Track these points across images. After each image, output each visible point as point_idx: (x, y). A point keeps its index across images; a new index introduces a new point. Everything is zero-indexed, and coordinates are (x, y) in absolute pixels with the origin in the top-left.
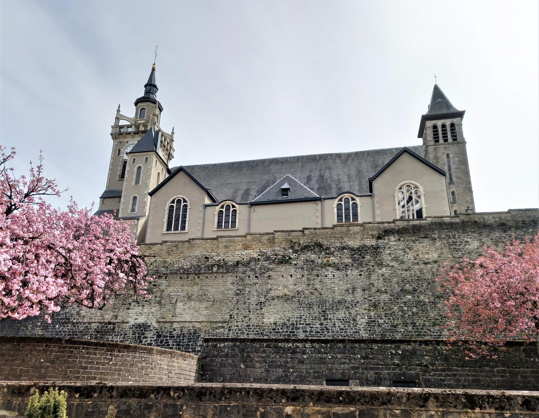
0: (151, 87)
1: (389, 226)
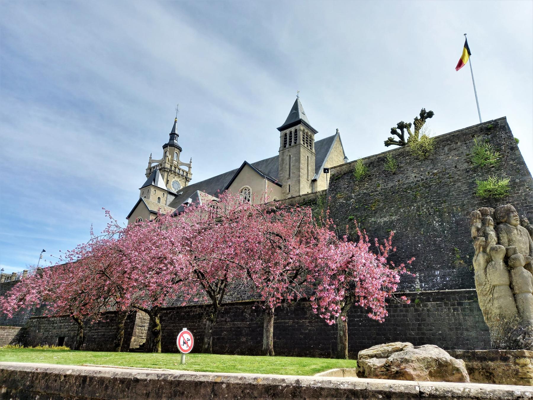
1: (342, 170)
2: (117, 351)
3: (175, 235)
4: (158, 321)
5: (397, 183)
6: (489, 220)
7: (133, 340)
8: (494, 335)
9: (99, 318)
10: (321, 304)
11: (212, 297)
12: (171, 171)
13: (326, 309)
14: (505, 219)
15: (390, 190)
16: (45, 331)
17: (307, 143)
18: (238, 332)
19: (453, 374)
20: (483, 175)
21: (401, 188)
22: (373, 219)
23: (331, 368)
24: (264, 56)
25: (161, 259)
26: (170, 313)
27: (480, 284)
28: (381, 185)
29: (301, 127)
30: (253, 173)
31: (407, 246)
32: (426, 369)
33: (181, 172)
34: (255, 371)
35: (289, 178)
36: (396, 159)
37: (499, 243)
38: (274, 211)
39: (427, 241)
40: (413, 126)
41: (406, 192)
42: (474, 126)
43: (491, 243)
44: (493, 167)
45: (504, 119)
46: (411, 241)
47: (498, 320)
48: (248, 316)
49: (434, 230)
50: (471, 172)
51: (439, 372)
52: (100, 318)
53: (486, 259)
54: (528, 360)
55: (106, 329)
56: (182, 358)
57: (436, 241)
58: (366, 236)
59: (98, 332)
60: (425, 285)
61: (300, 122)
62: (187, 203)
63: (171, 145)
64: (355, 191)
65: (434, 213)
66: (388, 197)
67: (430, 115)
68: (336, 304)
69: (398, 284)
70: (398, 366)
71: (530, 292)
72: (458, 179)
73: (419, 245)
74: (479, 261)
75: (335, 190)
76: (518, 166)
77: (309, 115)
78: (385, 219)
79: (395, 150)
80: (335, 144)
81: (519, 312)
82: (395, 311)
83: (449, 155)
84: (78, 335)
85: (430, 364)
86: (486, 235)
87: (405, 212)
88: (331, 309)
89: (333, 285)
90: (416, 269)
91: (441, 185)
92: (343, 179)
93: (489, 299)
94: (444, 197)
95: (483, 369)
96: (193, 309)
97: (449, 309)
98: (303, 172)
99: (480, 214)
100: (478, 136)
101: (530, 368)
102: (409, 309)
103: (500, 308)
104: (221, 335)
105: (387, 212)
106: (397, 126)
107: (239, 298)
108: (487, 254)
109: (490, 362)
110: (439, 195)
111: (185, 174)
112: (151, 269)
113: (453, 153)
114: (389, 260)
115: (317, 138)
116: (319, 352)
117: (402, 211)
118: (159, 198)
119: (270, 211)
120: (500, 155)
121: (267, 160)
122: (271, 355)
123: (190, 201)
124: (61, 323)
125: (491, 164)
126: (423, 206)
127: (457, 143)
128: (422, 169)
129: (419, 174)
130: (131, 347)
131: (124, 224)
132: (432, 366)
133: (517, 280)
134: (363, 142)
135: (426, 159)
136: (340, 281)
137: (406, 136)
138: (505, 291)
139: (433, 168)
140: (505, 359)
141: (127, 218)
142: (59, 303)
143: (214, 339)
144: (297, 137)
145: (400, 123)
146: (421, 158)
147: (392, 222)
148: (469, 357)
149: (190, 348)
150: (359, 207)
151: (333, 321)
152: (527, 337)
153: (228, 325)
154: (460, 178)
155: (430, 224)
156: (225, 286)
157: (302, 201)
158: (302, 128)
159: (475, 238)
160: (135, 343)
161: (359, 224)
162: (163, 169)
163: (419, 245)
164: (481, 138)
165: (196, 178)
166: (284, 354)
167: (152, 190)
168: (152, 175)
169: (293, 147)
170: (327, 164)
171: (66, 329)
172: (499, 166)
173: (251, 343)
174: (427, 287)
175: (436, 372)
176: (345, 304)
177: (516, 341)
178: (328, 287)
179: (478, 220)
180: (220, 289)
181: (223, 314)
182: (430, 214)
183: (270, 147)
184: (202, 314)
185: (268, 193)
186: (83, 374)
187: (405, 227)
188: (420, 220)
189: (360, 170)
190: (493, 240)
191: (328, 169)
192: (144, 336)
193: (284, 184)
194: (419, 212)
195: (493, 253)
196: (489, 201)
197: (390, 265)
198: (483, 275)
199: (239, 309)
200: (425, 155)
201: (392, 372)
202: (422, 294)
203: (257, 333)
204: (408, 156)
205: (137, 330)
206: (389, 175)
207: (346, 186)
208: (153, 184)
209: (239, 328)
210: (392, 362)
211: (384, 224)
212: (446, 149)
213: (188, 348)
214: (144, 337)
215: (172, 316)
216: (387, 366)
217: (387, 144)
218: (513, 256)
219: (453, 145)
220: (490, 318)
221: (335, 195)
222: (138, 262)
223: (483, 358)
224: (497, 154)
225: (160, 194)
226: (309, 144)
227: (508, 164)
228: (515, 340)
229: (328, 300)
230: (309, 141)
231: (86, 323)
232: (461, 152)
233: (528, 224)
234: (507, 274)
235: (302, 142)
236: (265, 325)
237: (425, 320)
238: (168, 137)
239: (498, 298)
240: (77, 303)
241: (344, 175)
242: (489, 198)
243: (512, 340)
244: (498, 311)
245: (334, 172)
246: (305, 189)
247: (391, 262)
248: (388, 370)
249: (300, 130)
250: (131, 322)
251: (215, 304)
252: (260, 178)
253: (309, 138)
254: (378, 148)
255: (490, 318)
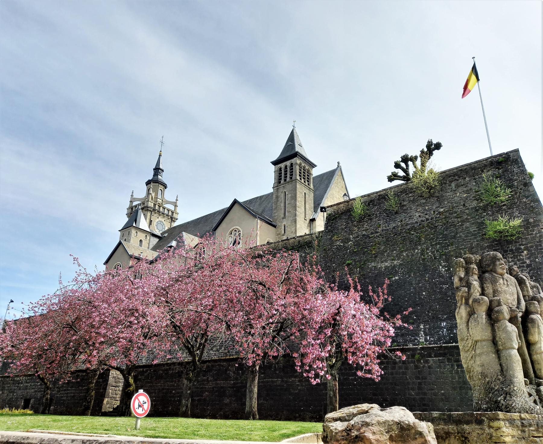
0: (157, 170)
1: (339, 209)
2: (87, 415)
3: (149, 285)
4: (131, 381)
5: (400, 223)
6: (473, 268)
7: (106, 400)
8: (477, 394)
9: (68, 378)
10: (305, 361)
11: (191, 353)
12: (154, 210)
13: (310, 366)
14: (491, 267)
15: (392, 231)
16: (10, 392)
17: (304, 178)
18: (221, 393)
19: (416, 438)
20: (493, 213)
21: (404, 229)
22: (373, 264)
23: (304, 433)
24: (262, 80)
25: (133, 311)
26: (147, 371)
27: (462, 340)
28: (381, 226)
29: (297, 160)
30: (243, 212)
31: (410, 294)
32: (386, 432)
33: (166, 212)
34: (215, 437)
35: (284, 217)
36: (398, 196)
37: (483, 294)
38: (260, 256)
39: (432, 288)
40: (419, 159)
41: (410, 233)
42: (483, 160)
43: (474, 294)
44: (504, 205)
45: (517, 151)
46: (415, 288)
47: (480, 379)
48: (232, 374)
49: (440, 276)
50: (480, 211)
51: (401, 436)
52: (70, 377)
53: (469, 312)
54: (502, 423)
55: (75, 390)
56: (137, 422)
57: (442, 288)
58: (358, 284)
59: (67, 393)
60: (430, 338)
61: (296, 155)
62: (171, 247)
63: (155, 181)
64: (354, 232)
65: (440, 257)
66: (391, 240)
67: (438, 146)
68: (322, 361)
69: (392, 337)
70: (358, 430)
71: (515, 349)
72: (466, 218)
73: (424, 293)
74: (462, 313)
75: (332, 232)
76: (532, 204)
77: (307, 147)
78: (386, 264)
79: (397, 186)
80: (336, 178)
81: (502, 370)
82: (394, 368)
83: (456, 192)
84: (44, 396)
85: (391, 428)
86: (469, 285)
87: (408, 256)
88: (315, 367)
89: (318, 339)
90: (420, 320)
91: (447, 225)
92: (341, 219)
93: (471, 356)
94: (451, 239)
95: (458, 433)
96: (172, 367)
97: (452, 365)
98: (300, 210)
99: (464, 262)
100: (488, 171)
101: (504, 432)
102: (408, 365)
103: (483, 365)
104: (202, 396)
105: (388, 256)
106: (401, 160)
107: (226, 353)
108: (470, 307)
109: (465, 426)
110: (445, 237)
111: (170, 214)
112: (120, 322)
113: (460, 189)
114: (382, 312)
115: (315, 172)
116: (310, 415)
117: (405, 255)
118: (141, 241)
119: (257, 257)
120: (512, 192)
121: (261, 197)
122: (254, 419)
123: (174, 243)
124: (27, 383)
125: (502, 202)
126: (427, 249)
127: (465, 178)
128: (427, 208)
129: (423, 213)
130: (103, 411)
131: (102, 269)
132: (393, 430)
133: (500, 335)
134: (365, 178)
135: (431, 196)
136: (326, 335)
137: (411, 170)
138: (487, 347)
139: (439, 207)
140: (480, 422)
141: (104, 264)
142: (23, 361)
143: (193, 400)
144: (292, 172)
145: (404, 156)
146: (425, 195)
147: (395, 266)
148: (445, 419)
149: (146, 411)
150: (358, 251)
151: (318, 380)
152: (508, 398)
153: (210, 386)
154: (469, 217)
155: (436, 269)
156: (206, 341)
157: (296, 244)
158: (298, 162)
159: (457, 288)
160: (108, 406)
161: (358, 269)
162: (145, 209)
163: (424, 293)
164: (490, 173)
165: (183, 218)
166: (271, 417)
167: (133, 231)
168: (133, 215)
169: (288, 182)
170: (327, 202)
171: (33, 390)
172: (511, 205)
173: (235, 405)
174: (432, 341)
175: (397, 436)
176: (336, 361)
177: (497, 402)
178: (313, 342)
179: (461, 269)
180: (200, 344)
181: (205, 373)
182: (435, 258)
183: (262, 182)
184: (182, 372)
185: (261, 235)
186: (11, 441)
187: (409, 273)
188: (425, 266)
189: (358, 208)
190: (476, 291)
191: (324, 208)
192: (118, 397)
193: (278, 224)
194: (424, 256)
195: (476, 306)
196: (500, 243)
197: (384, 317)
198: (465, 330)
199: (222, 366)
200: (429, 192)
201: (352, 436)
202: (422, 349)
203: (240, 393)
204: (411, 193)
205: (110, 391)
206: (390, 214)
207: (343, 227)
208: (134, 225)
209: (222, 387)
210: (353, 425)
211: (385, 270)
212: (453, 185)
213: (144, 411)
214: (118, 399)
215: (148, 374)
216: (348, 431)
217: (390, 179)
218: (496, 309)
219: (461, 181)
220: (472, 376)
221: (332, 237)
222: (107, 314)
223: (458, 422)
224: (508, 191)
225: (141, 236)
226: (306, 179)
227: (521, 202)
228: (496, 401)
229: (311, 356)
230: (306, 176)
231: (55, 383)
232: (469, 188)
233: (518, 273)
234: (489, 329)
235: (298, 178)
236: (248, 385)
237: (426, 379)
238: (152, 173)
239: (480, 355)
240: (42, 360)
241: (341, 216)
242: (499, 240)
243: (493, 401)
244: (479, 369)
245: (329, 211)
246: (302, 230)
247: (386, 313)
248: (348, 434)
249: (296, 164)
250: (103, 382)
251: (194, 361)
252: (252, 217)
253: (306, 173)
254: (381, 184)
255: (472, 376)
